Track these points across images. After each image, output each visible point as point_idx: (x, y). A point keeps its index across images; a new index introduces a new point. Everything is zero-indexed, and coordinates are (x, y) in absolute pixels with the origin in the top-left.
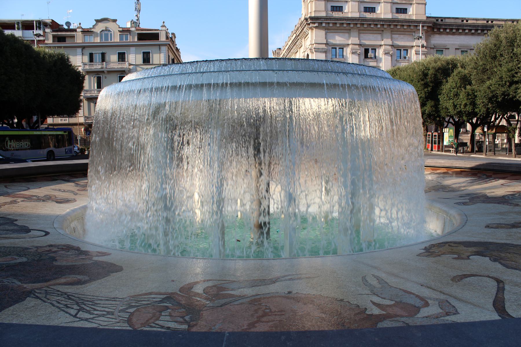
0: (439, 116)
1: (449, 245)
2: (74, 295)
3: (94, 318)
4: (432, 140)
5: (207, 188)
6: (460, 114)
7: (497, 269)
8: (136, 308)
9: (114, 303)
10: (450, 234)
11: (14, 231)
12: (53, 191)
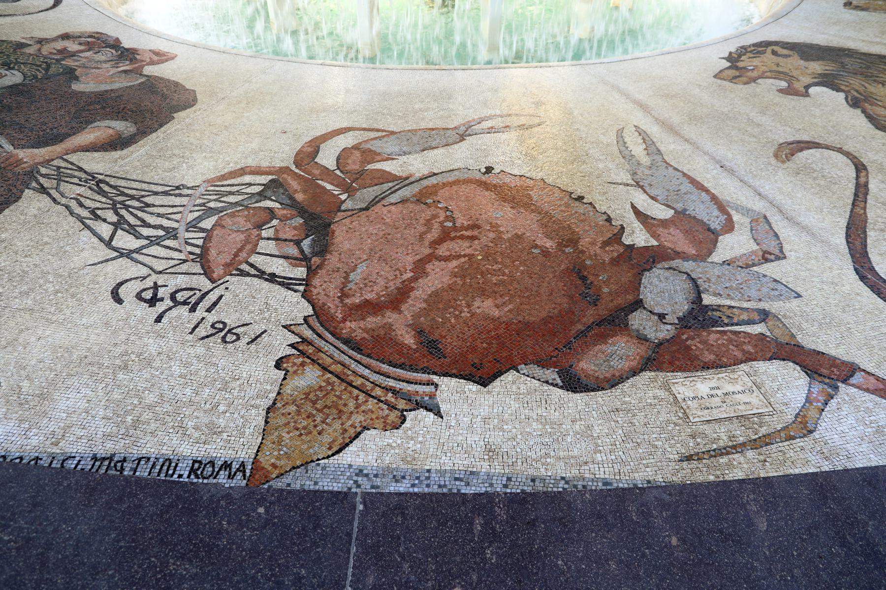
1: (774, 53)
2: (108, 179)
3: (143, 247)
8: (215, 218)
9: (177, 201)
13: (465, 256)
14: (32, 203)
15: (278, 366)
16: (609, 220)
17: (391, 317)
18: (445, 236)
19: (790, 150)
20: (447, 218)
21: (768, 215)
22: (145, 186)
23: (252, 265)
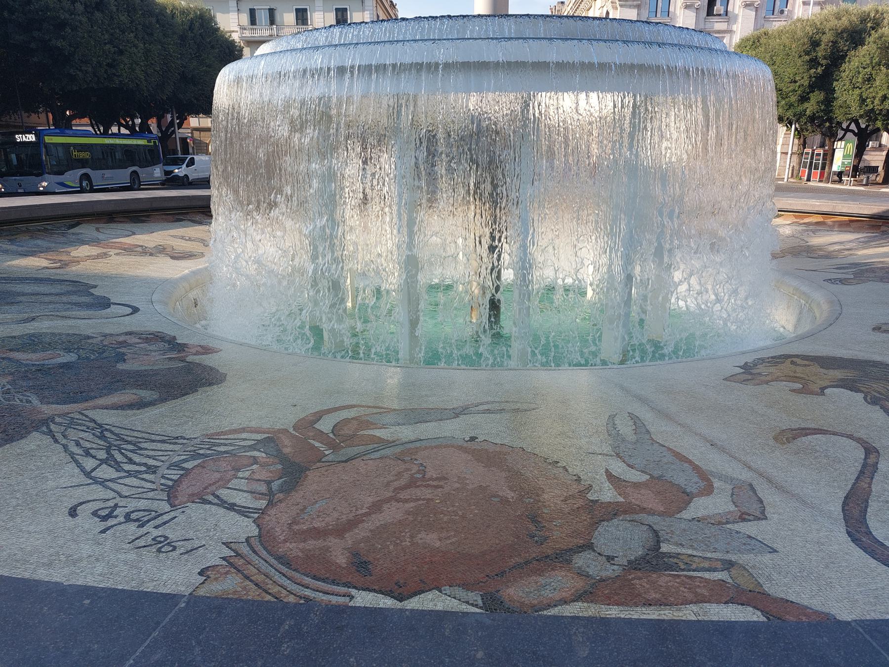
0: (830, 120)
1: (793, 363)
2: (113, 429)
4: (811, 163)
5: (393, 240)
6: (871, 115)
7: (870, 419)
9: (171, 447)
10: (801, 338)
11: (89, 306)
12: (172, 238)
13: (423, 499)
14: (35, 441)
15: (201, 573)
16: (579, 480)
17: (333, 542)
18: (412, 483)
19: (790, 436)
20: (418, 472)
21: (754, 483)
22: (144, 435)
23: (218, 497)
